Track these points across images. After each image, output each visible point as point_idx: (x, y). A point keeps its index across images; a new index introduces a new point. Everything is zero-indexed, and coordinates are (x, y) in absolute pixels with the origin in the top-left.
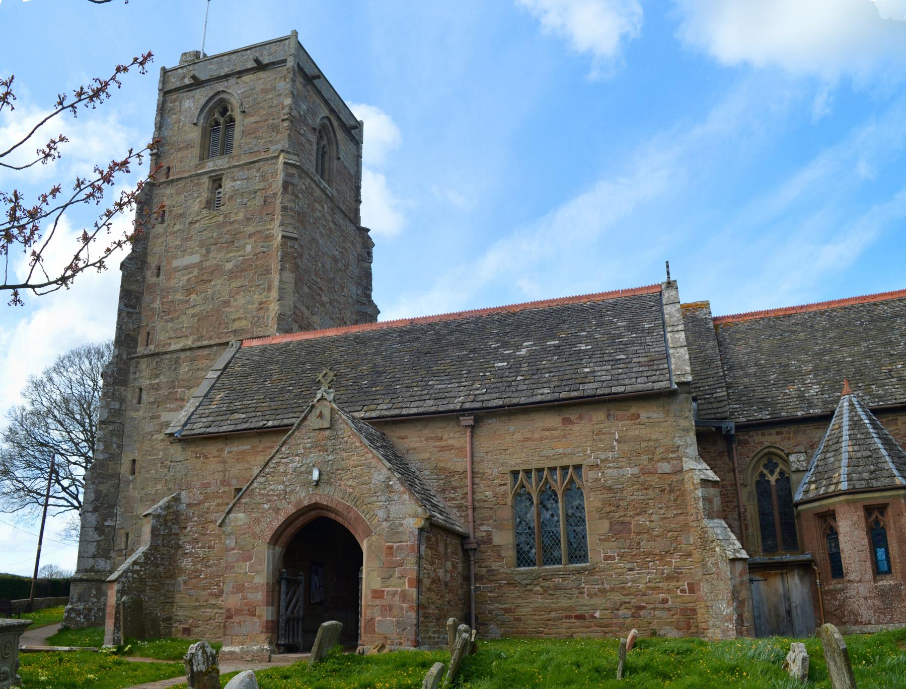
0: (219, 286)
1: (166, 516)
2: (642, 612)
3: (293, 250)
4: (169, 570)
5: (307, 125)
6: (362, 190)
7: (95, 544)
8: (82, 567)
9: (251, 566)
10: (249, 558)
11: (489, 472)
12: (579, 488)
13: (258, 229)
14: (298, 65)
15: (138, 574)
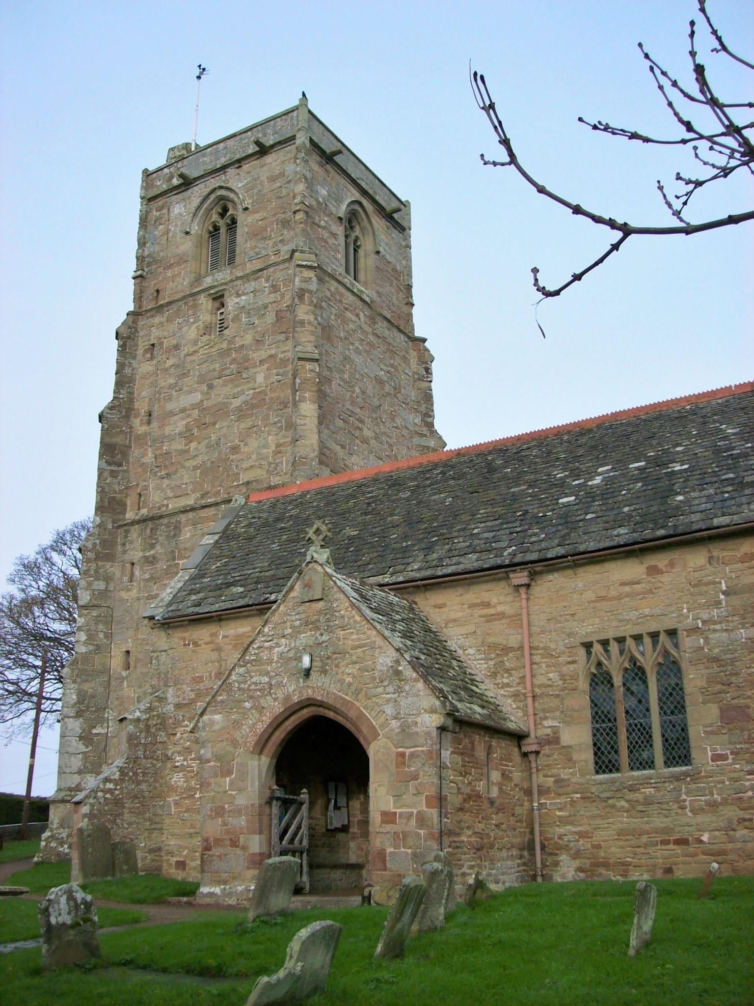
1: (148, 719)
3: (313, 375)
4: (156, 788)
5: (330, 215)
6: (413, 290)
7: (80, 756)
8: (63, 785)
9: (231, 783)
10: (229, 773)
11: (553, 646)
12: (674, 662)
13: (269, 352)
14: (311, 140)
15: (112, 794)
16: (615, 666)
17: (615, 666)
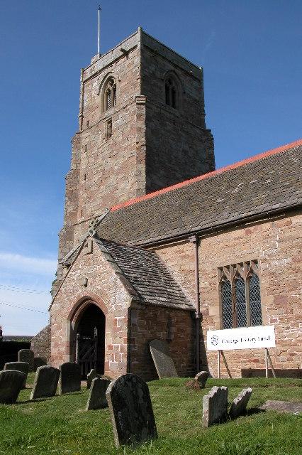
0: (112, 180)
2: (294, 358)
16: (230, 278)
17: (230, 278)
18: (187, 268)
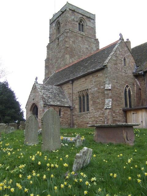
0: (59, 61)
18: (69, 92)
